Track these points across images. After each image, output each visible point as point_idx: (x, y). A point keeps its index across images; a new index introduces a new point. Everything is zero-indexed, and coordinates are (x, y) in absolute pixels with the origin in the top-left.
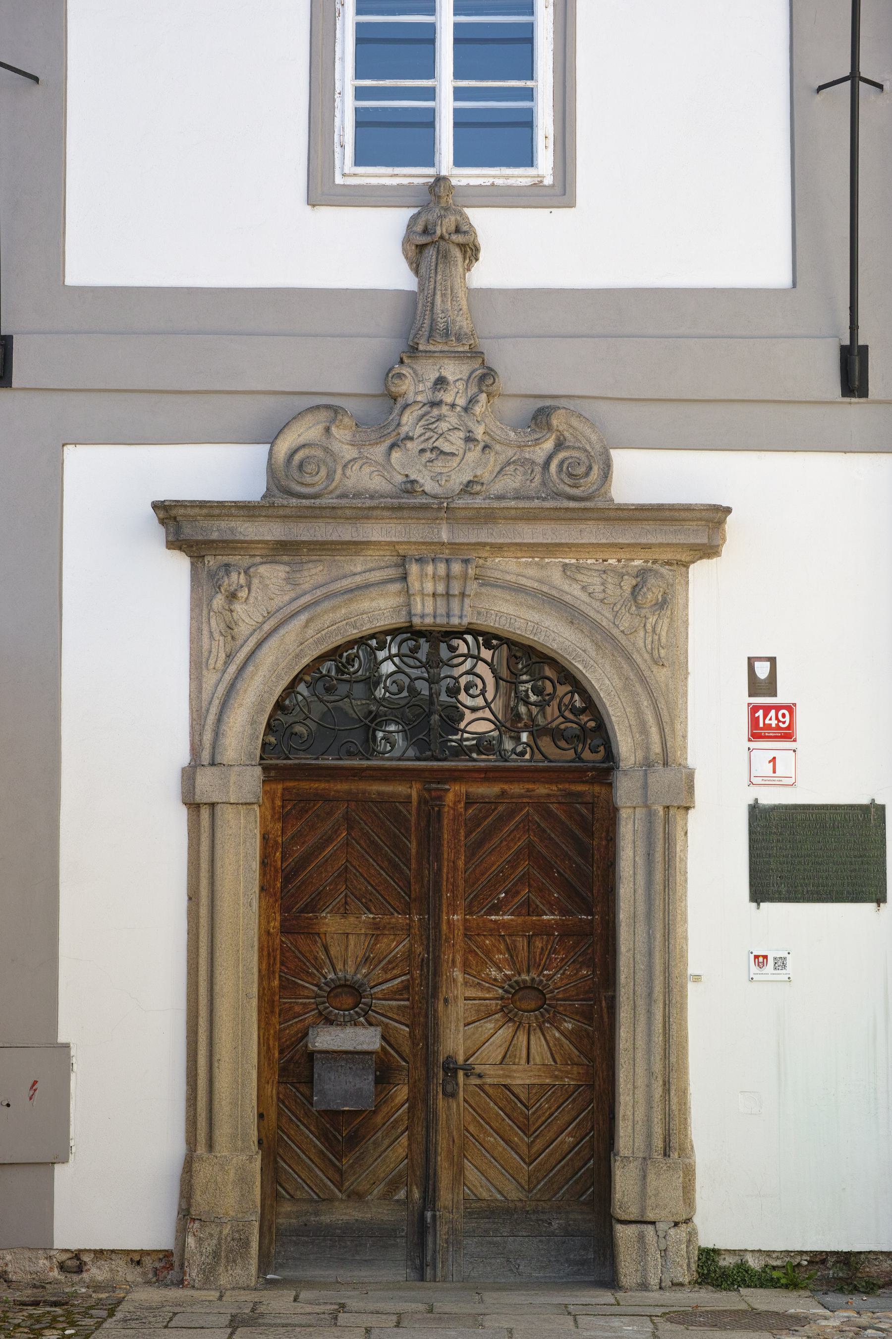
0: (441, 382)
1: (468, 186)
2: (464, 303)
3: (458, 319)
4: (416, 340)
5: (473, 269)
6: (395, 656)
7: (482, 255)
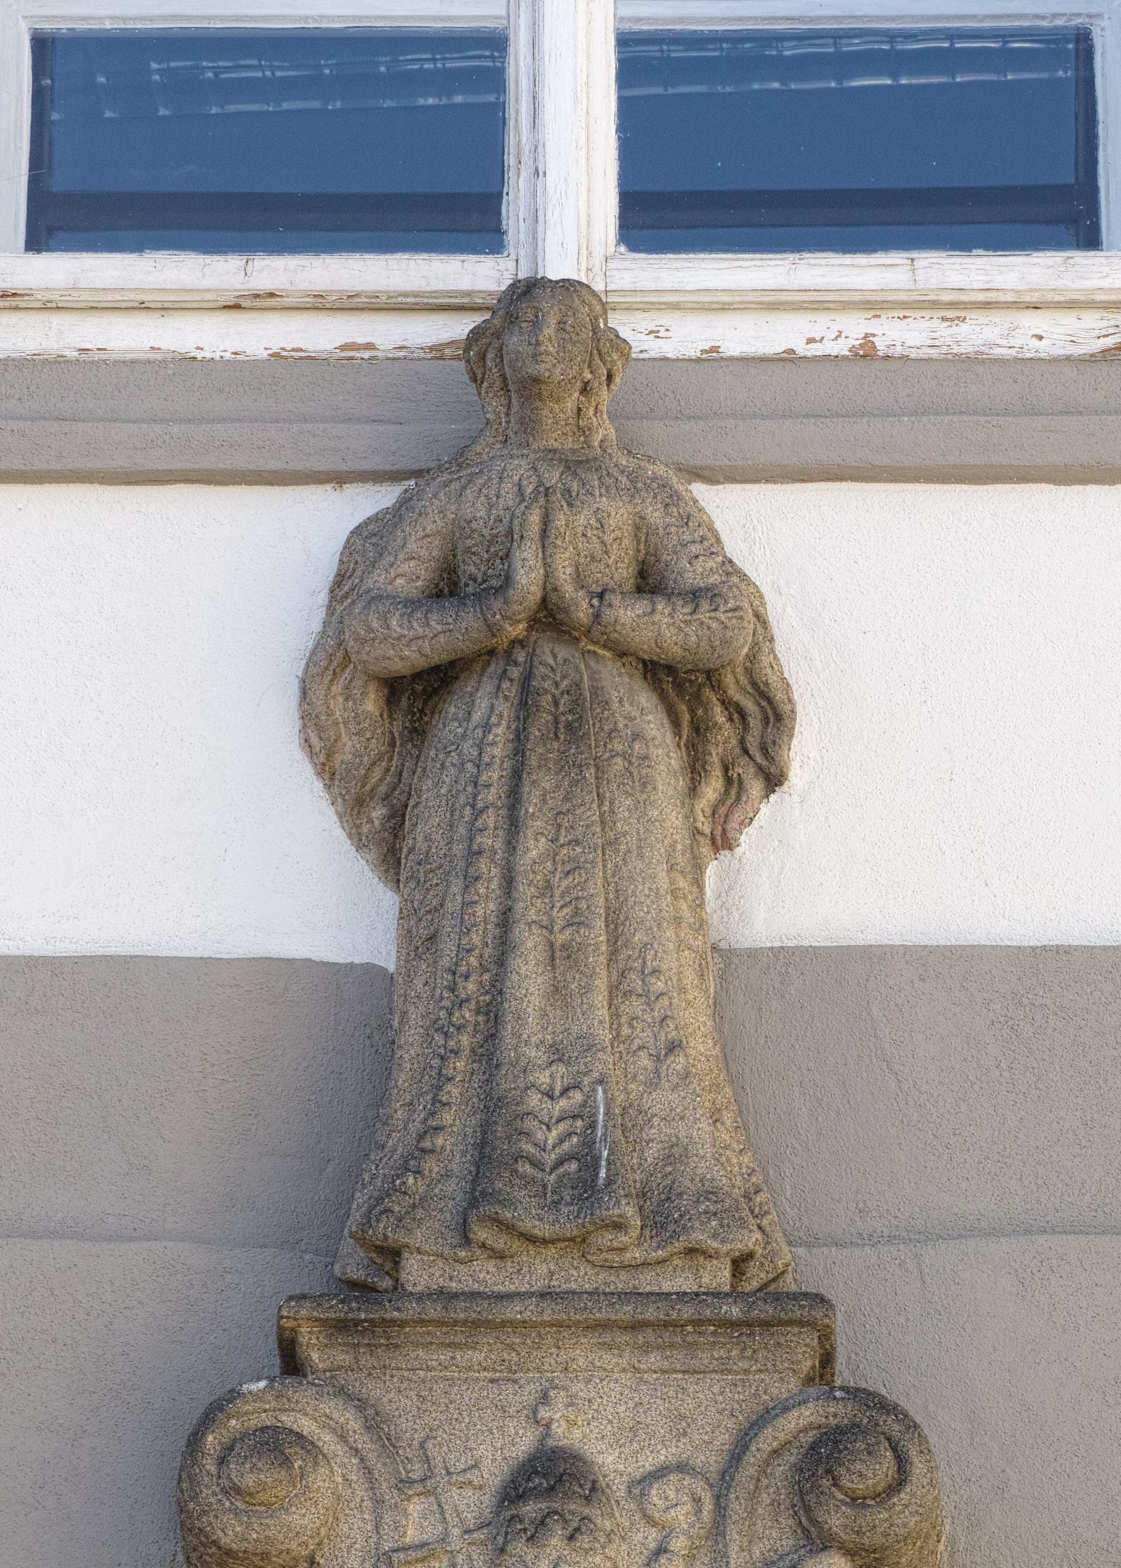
1: (712, 359)
2: (695, 1019)
3: (661, 1101)
4: (383, 1228)
5: (748, 840)
7: (803, 753)
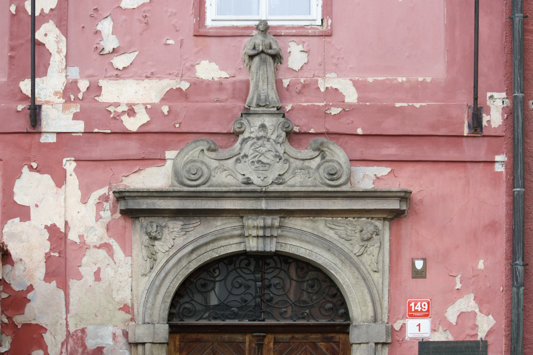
0: (263, 127)
6: (238, 268)
